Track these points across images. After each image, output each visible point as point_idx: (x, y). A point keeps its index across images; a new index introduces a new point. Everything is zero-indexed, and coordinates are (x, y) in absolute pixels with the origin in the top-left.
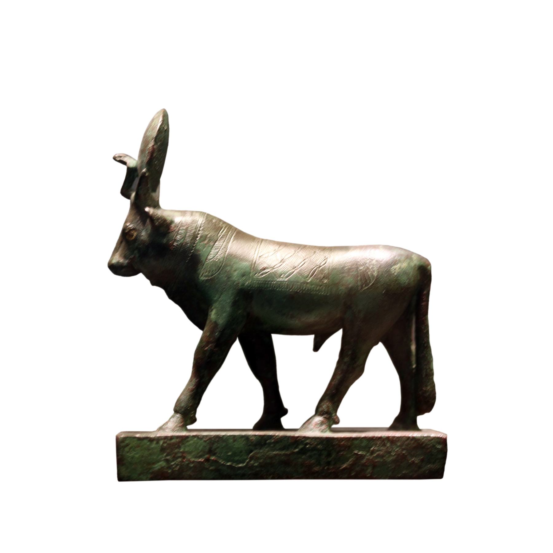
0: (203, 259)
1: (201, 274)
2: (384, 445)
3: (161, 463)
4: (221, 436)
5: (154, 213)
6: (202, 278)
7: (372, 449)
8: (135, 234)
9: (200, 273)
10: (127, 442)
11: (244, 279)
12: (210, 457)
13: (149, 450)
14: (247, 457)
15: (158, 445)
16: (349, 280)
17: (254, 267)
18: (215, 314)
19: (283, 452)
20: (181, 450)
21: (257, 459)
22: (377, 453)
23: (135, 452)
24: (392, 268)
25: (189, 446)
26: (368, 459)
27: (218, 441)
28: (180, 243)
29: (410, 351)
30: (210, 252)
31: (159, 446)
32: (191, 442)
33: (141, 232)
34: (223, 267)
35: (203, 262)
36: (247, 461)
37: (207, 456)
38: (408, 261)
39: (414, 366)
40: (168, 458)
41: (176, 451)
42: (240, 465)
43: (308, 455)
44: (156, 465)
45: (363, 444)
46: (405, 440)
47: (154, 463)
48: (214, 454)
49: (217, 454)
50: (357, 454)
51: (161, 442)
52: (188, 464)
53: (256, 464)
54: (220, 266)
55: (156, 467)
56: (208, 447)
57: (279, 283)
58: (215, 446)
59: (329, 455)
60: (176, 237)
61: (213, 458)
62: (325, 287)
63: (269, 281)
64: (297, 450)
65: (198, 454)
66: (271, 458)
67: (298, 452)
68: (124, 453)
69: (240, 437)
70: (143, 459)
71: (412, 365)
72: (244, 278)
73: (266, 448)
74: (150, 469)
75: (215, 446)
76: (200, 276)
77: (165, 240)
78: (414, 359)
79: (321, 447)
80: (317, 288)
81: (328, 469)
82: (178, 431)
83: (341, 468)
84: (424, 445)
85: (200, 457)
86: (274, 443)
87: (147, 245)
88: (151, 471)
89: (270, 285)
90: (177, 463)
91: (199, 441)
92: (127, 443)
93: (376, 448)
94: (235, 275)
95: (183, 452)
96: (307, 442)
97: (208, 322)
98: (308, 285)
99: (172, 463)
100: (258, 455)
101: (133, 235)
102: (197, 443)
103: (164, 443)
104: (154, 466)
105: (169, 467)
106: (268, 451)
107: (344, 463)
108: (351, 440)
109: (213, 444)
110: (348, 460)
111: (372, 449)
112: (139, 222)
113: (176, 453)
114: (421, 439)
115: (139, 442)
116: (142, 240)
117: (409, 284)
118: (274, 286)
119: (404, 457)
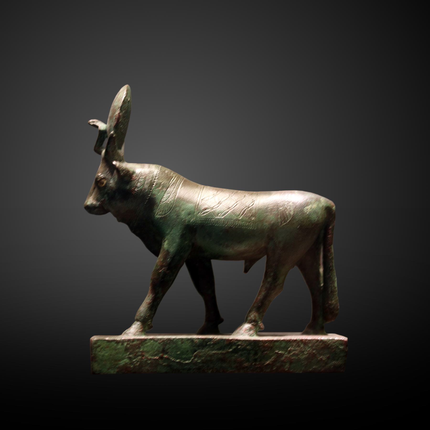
0: (158, 201)
1: (156, 213)
2: (299, 346)
3: (125, 360)
4: (172, 339)
5: (119, 165)
6: (157, 216)
7: (289, 349)
8: (105, 182)
9: (155, 213)
10: (99, 344)
11: (190, 217)
12: (163, 355)
13: (116, 350)
14: (192, 356)
15: (123, 346)
16: (272, 218)
17: (197, 208)
18: (167, 244)
19: (220, 352)
20: (141, 350)
21: (200, 357)
22: (293, 352)
23: (105, 352)
24: (305, 208)
25: (147, 347)
26: (286, 357)
27: (169, 343)
28: (140, 189)
29: (319, 273)
30: (164, 196)
31: (123, 347)
32: (149, 344)
33: (110, 181)
34: (174, 207)
35: (158, 204)
36: (192, 358)
37: (161, 355)
38: (317, 203)
39: (322, 285)
40: (131, 356)
41: (137, 350)
42: (187, 362)
43: (239, 353)
44: (122, 362)
45: (283, 345)
46: (315, 342)
47: (120, 360)
48: (167, 353)
50: (277, 353)
51: (125, 344)
52: (146, 361)
53: (199, 361)
54: (171, 207)
55: (122, 363)
56: (161, 348)
57: (217, 220)
58: (167, 347)
59: (256, 354)
60: (137, 184)
61: (165, 356)
62: (252, 223)
63: (209, 219)
64: (231, 350)
65: (154, 353)
66: (211, 356)
67: (231, 352)
68: (96, 353)
69: (186, 340)
70: (111, 357)
71: (320, 284)
72: (190, 216)
73: (207, 348)
74: (117, 364)
75: (167, 347)
76: (156, 215)
77: (128, 187)
78: (322, 279)
79: (250, 347)
80: (246, 224)
81: (255, 365)
83: (265, 364)
84: (330, 346)
85: (156, 355)
86: (213, 344)
87: (114, 190)
88: (117, 366)
89: (210, 222)
91: (154, 343)
92: (99, 345)
93: (292, 349)
94: (183, 214)
95: (142, 352)
96: (239, 344)
97: (161, 251)
98: (240, 222)
99: (134, 360)
100: (201, 354)
101: (103, 183)
102: (153, 345)
103: (127, 344)
104: (119, 363)
105: (131, 364)
106: (208, 351)
107: (267, 360)
108: (273, 342)
109: (166, 345)
110: (270, 357)
111: (289, 349)
112: (108, 172)
113: (137, 353)
114: (327, 341)
115: (108, 343)
116: (110, 186)
117: (318, 221)
118: (213, 223)
119: (314, 355)
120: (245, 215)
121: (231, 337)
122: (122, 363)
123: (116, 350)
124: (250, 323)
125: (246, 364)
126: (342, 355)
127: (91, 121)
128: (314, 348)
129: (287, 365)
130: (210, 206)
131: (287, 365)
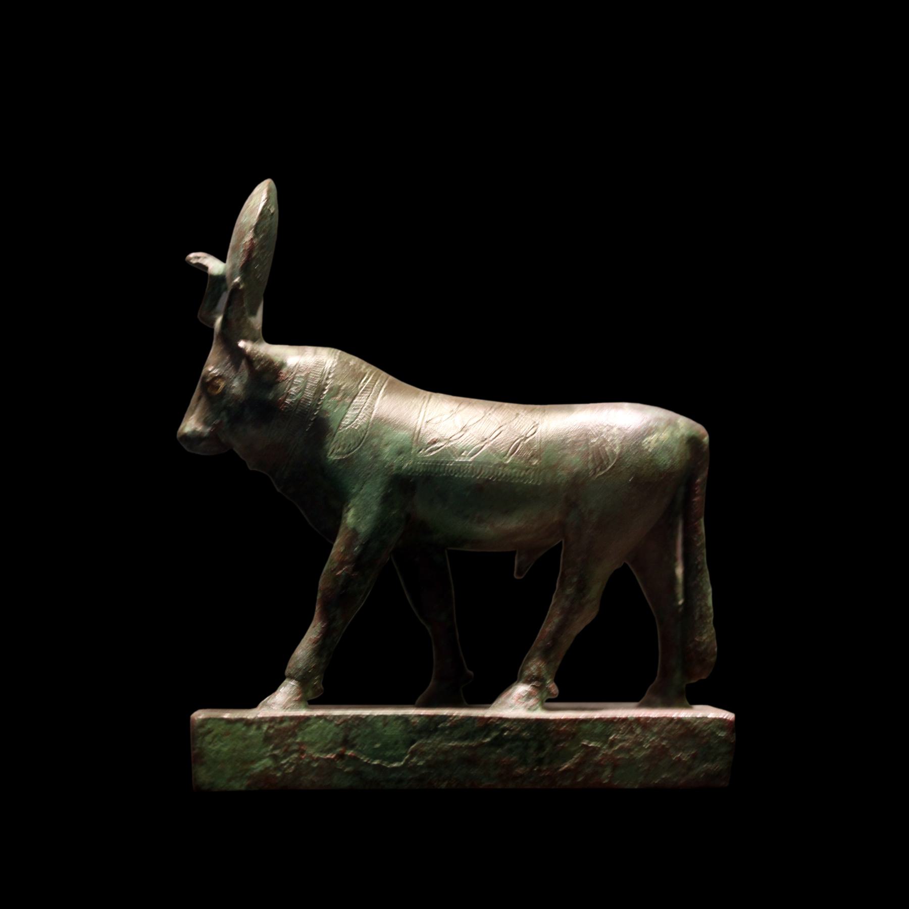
0: (334, 425)
1: (331, 451)
2: (632, 731)
3: (264, 761)
4: (364, 717)
6: (332, 457)
7: (611, 738)
9: (328, 449)
10: (209, 726)
11: (401, 459)
12: (345, 751)
13: (245, 739)
14: (407, 752)
15: (260, 732)
16: (574, 461)
17: (417, 439)
18: (354, 515)
19: (466, 743)
20: (298, 740)
21: (423, 754)
22: (620, 744)
23: (221, 744)
25: (310, 733)
27: (358, 725)
28: (296, 400)
29: (673, 576)
30: (346, 413)
31: (261, 733)
32: (314, 727)
33: (232, 382)
35: (334, 431)
36: (407, 757)
37: (340, 749)
38: (671, 429)
39: (681, 602)
40: (276, 752)
41: (289, 741)
42: (395, 765)
43: (506, 747)
44: (257, 765)
45: (597, 730)
46: (665, 723)
47: (253, 762)
48: (352, 747)
49: (357, 746)
50: (586, 746)
51: (265, 727)
52: (309, 763)
53: (421, 763)
54: (361, 438)
55: (257, 768)
56: (341, 736)
57: (459, 465)
58: (354, 733)
59: (541, 748)
60: (289, 389)
61: (349, 753)
63: (442, 462)
64: (488, 740)
65: (325, 746)
66: (446, 752)
67: (489, 744)
68: (204, 745)
69: (394, 718)
70: (235, 754)
71: (677, 600)
72: (401, 457)
73: (438, 736)
74: (247, 770)
75: (354, 733)
76: (329, 453)
77: (271, 394)
78: (680, 590)
79: (528, 734)
80: (520, 473)
81: (539, 771)
82: (292, 708)
83: (560, 770)
84: (697, 731)
85: (329, 751)
86: (450, 727)
87: (241, 402)
88: (248, 774)
89: (445, 468)
90: (290, 761)
91: (327, 724)
92: (209, 729)
93: (618, 737)
94: (387, 453)
95: (301, 744)
96: (505, 727)
97: (341, 530)
98: (506, 469)
99: (283, 762)
100: (425, 749)
101: (218, 387)
102: (324, 729)
103: (269, 728)
104: (252, 766)
105: (278, 768)
106: (441, 742)
107: (565, 761)
108: (577, 722)
109: (350, 729)
110: (571, 755)
111: (611, 738)
112: (229, 364)
113: (289, 745)
114: (692, 721)
115: (229, 726)
116: (233, 394)
117: (672, 467)
118: (450, 471)
119: (664, 751)
120: (519, 455)
122: (258, 767)
123: (245, 739)
124: (528, 682)
125: (520, 770)
126: (723, 749)
127: (192, 255)
128: (663, 735)
129: (607, 773)
130: (444, 436)
131: (607, 773)
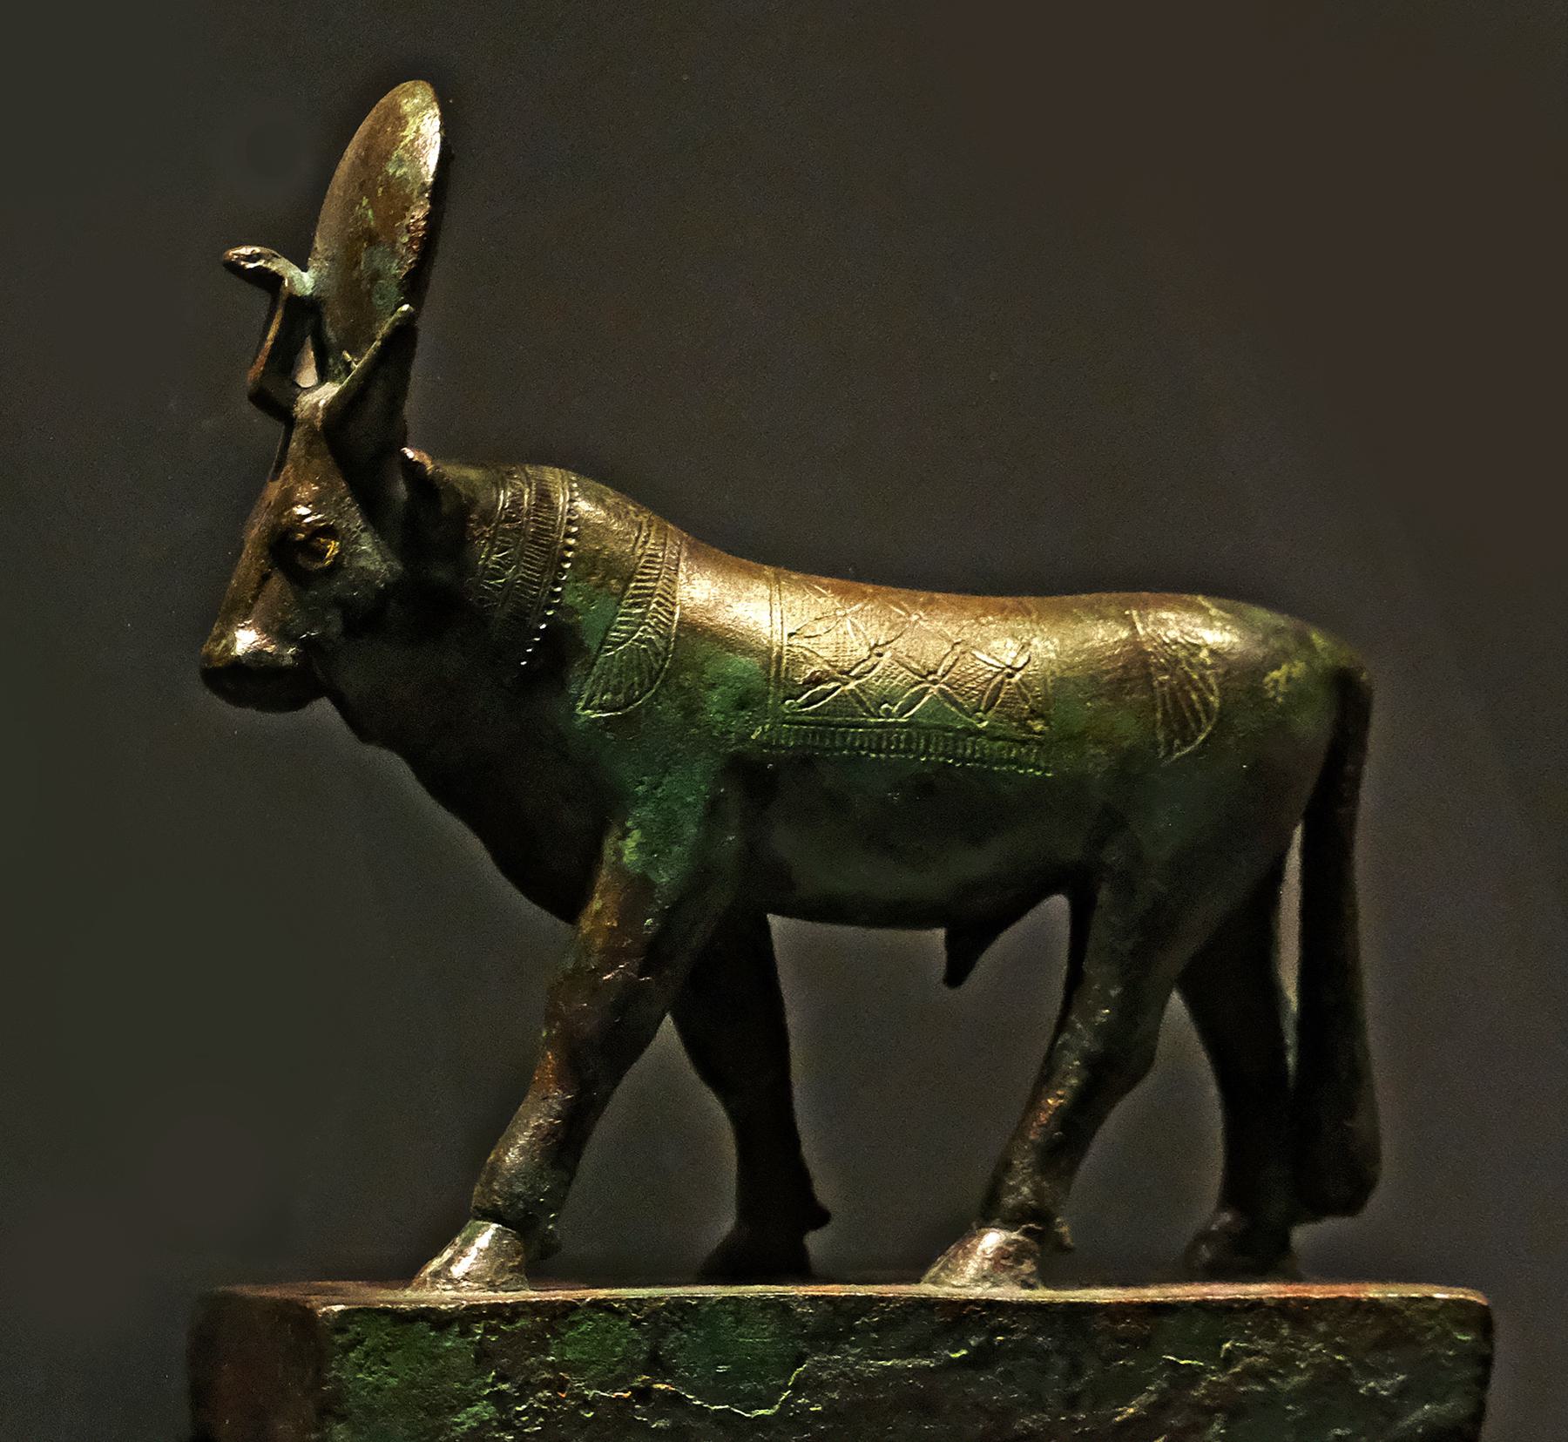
8: (333, 547)
13: (434, 1358)
17: (778, 672)
18: (639, 846)
21: (822, 1385)
25: (576, 1342)
47: (454, 1410)
66: (868, 1384)
75: (670, 1343)
82: (492, 1286)
86: (877, 1328)
97: (604, 876)
106: (860, 1357)
107: (1126, 1403)
115: (397, 1330)
121: (925, 1289)
123: (434, 1358)
124: (1009, 1224)
